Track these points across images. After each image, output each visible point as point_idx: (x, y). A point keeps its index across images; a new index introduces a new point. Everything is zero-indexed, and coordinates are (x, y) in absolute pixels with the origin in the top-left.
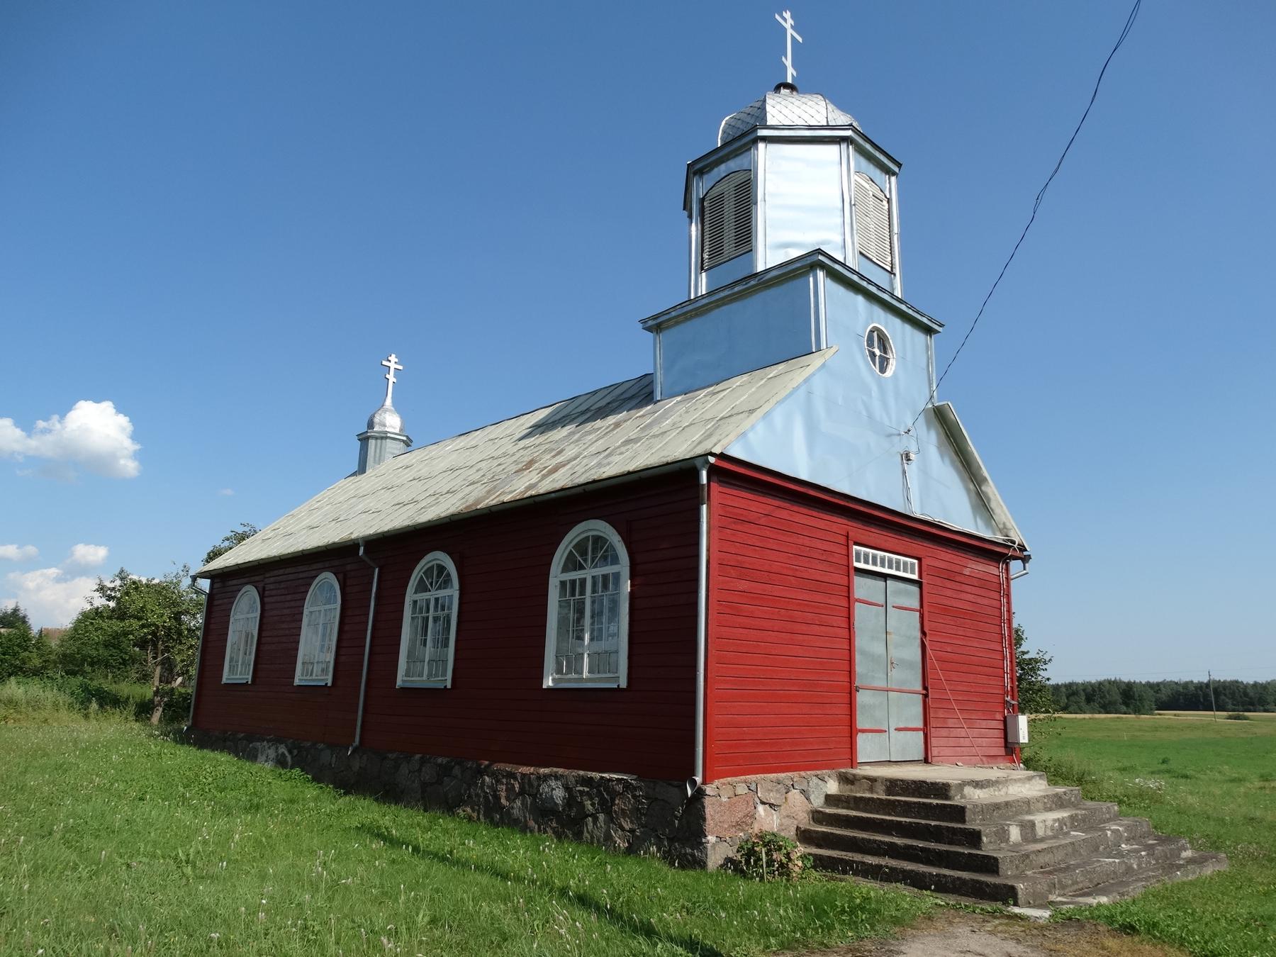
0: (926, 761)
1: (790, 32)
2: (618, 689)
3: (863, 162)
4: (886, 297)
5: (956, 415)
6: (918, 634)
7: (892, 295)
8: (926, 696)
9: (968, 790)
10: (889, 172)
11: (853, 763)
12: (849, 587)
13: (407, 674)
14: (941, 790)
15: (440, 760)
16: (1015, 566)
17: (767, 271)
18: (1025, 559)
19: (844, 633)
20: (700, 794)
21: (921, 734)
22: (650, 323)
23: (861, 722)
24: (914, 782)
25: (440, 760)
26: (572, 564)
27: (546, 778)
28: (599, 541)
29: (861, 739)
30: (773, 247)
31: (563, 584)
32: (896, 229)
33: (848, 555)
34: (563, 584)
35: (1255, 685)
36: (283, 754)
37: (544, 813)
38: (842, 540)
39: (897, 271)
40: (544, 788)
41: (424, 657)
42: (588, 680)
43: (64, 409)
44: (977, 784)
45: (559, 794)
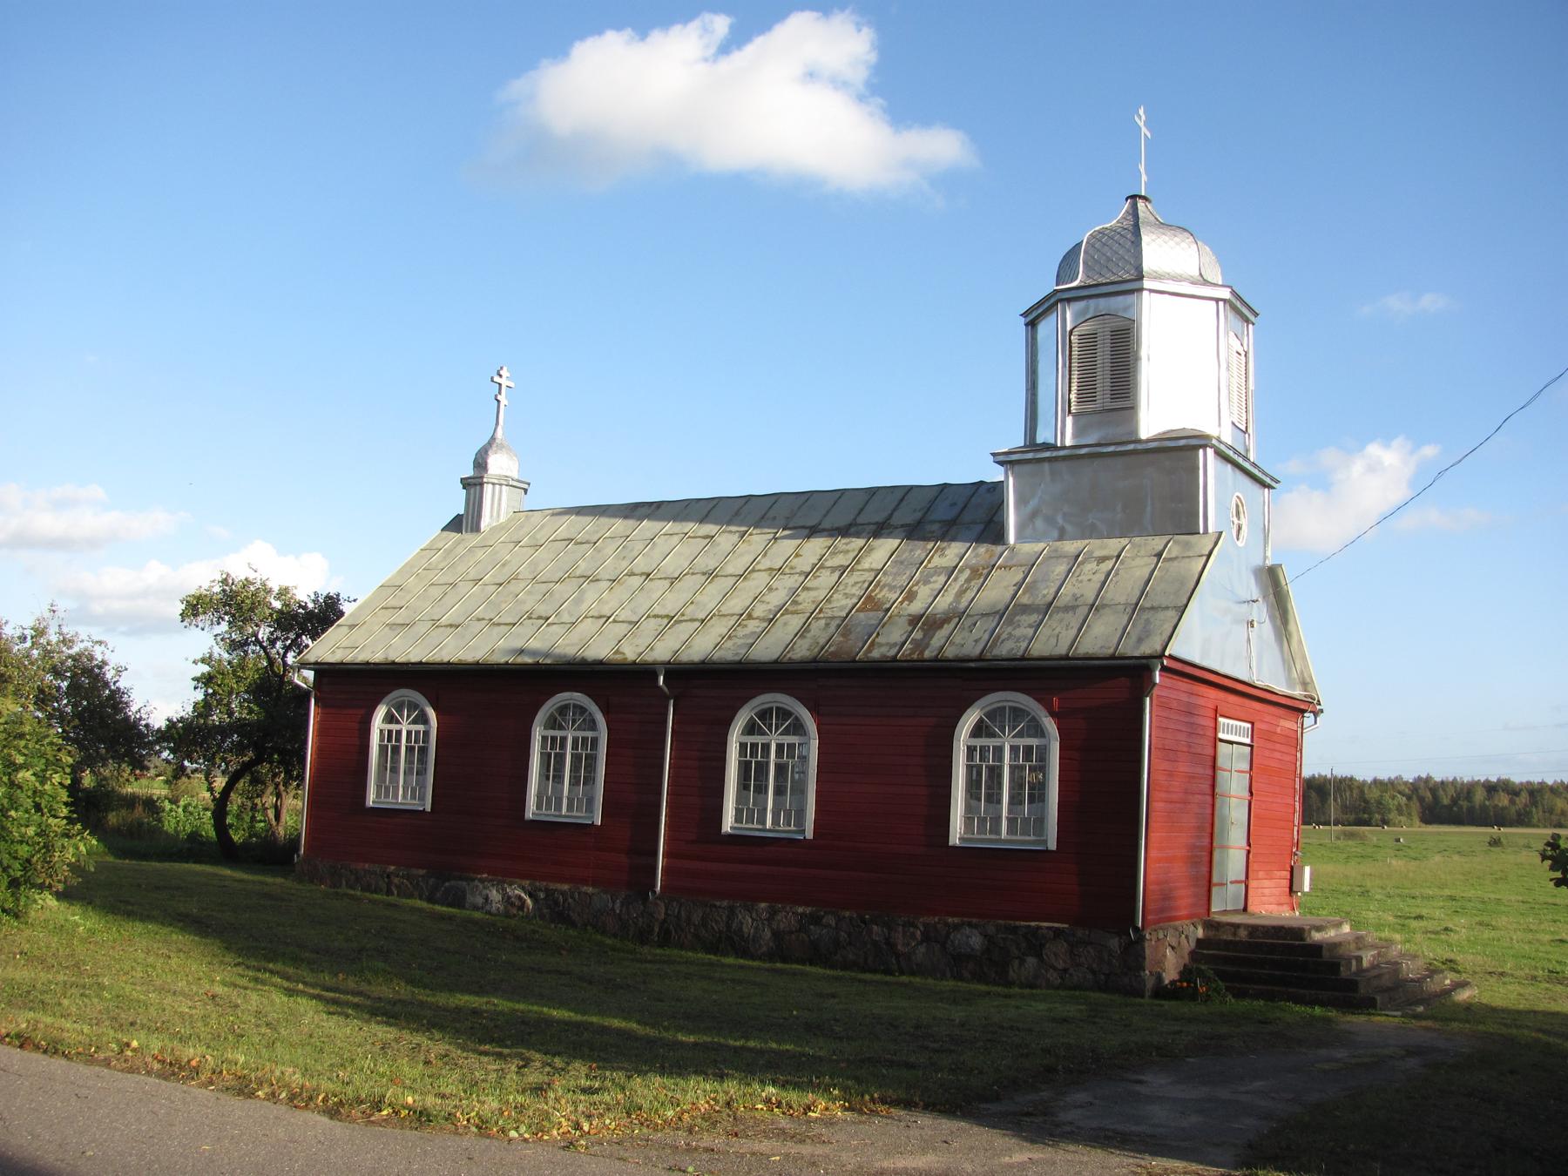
1: (1144, 129)
2: (1047, 851)
3: (1231, 315)
4: (1240, 460)
5: (1288, 576)
6: (1247, 794)
7: (1246, 458)
10: (1247, 321)
15: (800, 910)
16: (1309, 719)
17: (1148, 441)
18: (1316, 714)
19: (1209, 798)
20: (1141, 939)
22: (1001, 458)
24: (1274, 927)
25: (800, 910)
27: (956, 927)
29: (1215, 890)
30: (1156, 417)
32: (1251, 386)
33: (1216, 729)
35: (1376, 782)
37: (958, 964)
38: (1212, 714)
39: (1250, 430)
40: (957, 938)
42: (1006, 841)
45: (976, 941)
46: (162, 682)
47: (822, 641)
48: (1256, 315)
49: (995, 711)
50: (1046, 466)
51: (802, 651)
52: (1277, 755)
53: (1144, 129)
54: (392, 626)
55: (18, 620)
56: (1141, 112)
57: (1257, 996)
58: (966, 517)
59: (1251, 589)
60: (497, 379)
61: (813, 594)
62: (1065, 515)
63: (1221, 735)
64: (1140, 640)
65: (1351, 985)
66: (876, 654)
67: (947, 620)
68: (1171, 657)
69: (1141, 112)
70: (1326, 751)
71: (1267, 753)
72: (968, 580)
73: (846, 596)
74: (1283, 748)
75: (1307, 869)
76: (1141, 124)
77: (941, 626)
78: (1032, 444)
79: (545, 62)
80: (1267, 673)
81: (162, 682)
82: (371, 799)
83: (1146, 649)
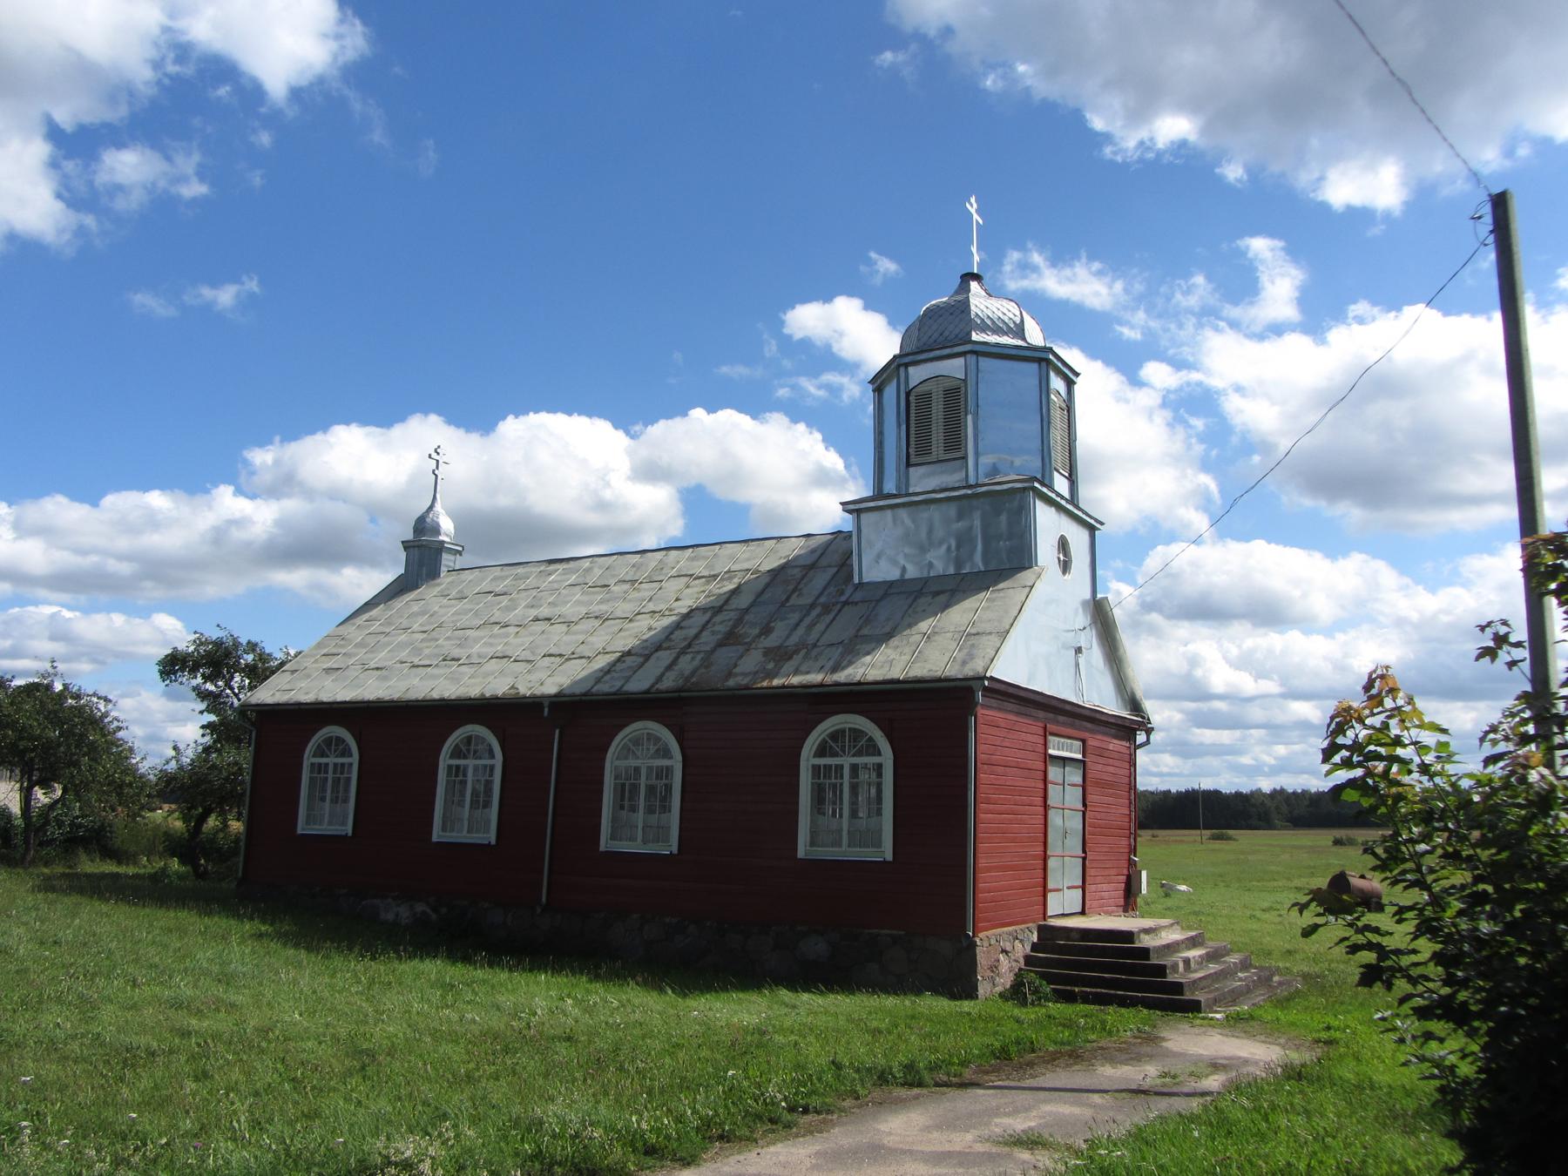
0: (1083, 913)
1: (976, 216)
2: (885, 862)
8: (1084, 859)
9: (1142, 936)
11: (1045, 918)
12: (1045, 773)
13: (613, 837)
14: (1128, 936)
21: (1080, 891)
22: (852, 507)
23: (1050, 885)
26: (320, 752)
28: (340, 740)
29: (1050, 896)
31: (450, 767)
34: (450, 767)
36: (424, 913)
41: (325, 814)
43: (321, 422)
44: (1147, 931)
46: (164, 728)
47: (687, 673)
48: (1077, 375)
49: (837, 732)
50: (889, 513)
51: (668, 683)
52: (1111, 769)
53: (976, 216)
54: (328, 670)
55: (23, 670)
56: (973, 200)
57: (1086, 999)
58: (823, 562)
59: (1082, 619)
60: (434, 455)
61: (684, 632)
62: (906, 555)
63: (1051, 752)
64: (964, 663)
65: (1178, 988)
66: (731, 683)
67: (796, 652)
68: (992, 679)
69: (973, 200)
70: (1159, 770)
71: (1100, 767)
72: (819, 616)
73: (713, 633)
74: (1117, 763)
75: (1144, 874)
76: (973, 211)
77: (790, 658)
78: (879, 494)
79: (818, 343)
80: (1100, 696)
81: (164, 728)
82: (302, 828)
83: (968, 671)
